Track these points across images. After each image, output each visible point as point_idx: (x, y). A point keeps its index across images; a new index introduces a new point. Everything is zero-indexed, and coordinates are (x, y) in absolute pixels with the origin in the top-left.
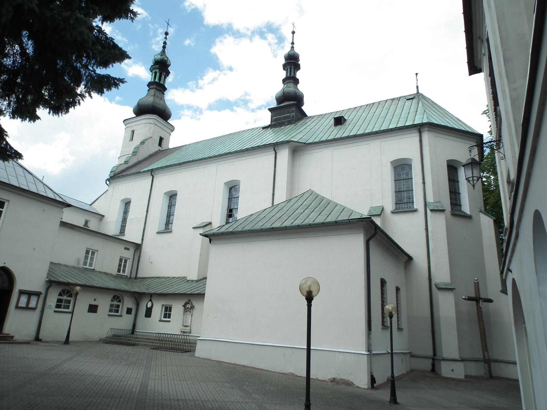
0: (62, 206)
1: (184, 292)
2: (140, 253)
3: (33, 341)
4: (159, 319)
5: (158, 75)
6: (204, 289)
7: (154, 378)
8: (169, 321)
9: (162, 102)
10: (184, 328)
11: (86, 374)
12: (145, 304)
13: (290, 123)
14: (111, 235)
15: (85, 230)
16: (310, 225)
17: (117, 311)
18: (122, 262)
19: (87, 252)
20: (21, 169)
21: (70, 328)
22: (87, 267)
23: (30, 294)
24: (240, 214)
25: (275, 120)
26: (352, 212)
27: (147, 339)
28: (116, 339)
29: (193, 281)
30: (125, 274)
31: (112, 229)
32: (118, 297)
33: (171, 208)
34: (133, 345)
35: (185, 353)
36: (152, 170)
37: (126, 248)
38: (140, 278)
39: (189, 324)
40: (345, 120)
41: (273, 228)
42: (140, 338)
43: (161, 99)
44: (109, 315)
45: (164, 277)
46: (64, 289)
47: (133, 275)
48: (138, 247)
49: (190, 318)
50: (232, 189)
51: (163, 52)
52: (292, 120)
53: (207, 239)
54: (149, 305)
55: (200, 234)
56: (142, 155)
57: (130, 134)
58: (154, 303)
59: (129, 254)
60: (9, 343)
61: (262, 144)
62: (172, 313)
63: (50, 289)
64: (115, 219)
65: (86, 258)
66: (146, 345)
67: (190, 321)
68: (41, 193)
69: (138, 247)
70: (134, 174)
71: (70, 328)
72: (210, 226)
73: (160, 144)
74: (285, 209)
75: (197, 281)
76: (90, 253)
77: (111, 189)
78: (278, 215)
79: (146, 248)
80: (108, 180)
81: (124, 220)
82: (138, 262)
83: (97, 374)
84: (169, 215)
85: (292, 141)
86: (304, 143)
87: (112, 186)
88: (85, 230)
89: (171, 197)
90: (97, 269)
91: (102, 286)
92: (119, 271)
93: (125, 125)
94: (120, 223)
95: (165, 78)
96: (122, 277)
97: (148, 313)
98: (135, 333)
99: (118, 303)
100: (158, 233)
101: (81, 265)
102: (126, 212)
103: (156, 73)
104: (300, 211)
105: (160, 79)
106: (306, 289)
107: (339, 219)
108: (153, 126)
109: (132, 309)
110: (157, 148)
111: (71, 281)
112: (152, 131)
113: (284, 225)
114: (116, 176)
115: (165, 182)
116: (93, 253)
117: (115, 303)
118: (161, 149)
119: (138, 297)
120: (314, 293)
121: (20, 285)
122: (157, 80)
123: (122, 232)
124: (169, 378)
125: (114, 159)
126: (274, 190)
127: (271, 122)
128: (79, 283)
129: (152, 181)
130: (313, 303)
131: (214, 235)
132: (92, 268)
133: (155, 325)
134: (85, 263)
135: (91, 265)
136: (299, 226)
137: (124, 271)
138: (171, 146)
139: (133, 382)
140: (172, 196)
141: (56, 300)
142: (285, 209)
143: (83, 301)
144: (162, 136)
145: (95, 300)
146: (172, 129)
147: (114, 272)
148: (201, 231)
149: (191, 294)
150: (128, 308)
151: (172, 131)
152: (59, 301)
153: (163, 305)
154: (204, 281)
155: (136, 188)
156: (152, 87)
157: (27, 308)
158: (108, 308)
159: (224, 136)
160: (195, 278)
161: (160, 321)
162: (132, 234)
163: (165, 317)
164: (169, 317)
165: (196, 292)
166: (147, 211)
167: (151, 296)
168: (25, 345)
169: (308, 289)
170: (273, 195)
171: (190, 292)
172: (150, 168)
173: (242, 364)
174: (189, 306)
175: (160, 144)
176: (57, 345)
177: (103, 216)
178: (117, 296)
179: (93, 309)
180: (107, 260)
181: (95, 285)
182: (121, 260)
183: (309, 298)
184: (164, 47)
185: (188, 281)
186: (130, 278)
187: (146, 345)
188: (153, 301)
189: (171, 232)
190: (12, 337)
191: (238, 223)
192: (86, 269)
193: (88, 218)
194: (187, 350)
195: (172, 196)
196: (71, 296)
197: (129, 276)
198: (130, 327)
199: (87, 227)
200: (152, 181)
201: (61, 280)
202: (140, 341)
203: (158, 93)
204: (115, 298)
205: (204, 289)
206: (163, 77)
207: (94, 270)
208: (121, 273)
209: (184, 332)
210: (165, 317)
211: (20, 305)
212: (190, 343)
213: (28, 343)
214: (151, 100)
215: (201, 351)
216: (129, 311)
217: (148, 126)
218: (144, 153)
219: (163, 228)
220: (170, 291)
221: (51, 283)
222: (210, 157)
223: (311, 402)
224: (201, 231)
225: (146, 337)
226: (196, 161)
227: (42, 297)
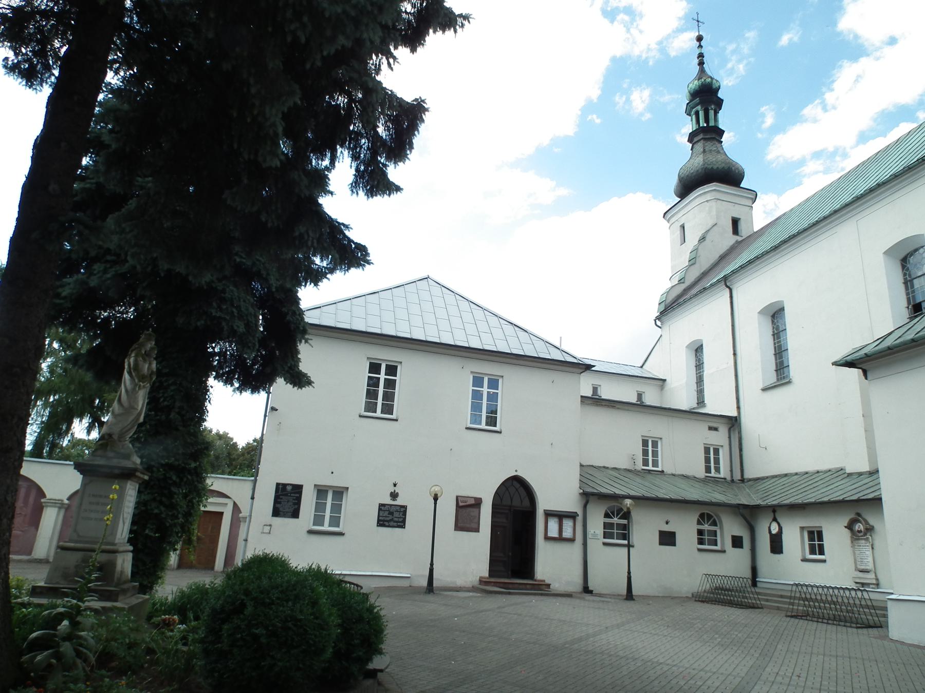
1: (841, 498)
2: (740, 432)
3: (581, 593)
4: (800, 558)
5: (701, 114)
6: (876, 482)
7: (771, 679)
8: (824, 561)
9: (720, 157)
10: (861, 575)
12: (765, 528)
15: (640, 406)
18: (710, 454)
19: (645, 443)
20: (511, 327)
21: (629, 573)
22: (650, 467)
23: (561, 516)
27: (782, 596)
28: (720, 595)
29: (860, 474)
30: (722, 475)
31: (683, 399)
32: (709, 517)
33: (779, 337)
34: (753, 607)
35: (865, 631)
36: (725, 278)
37: (710, 428)
38: (750, 480)
39: (870, 566)
42: (765, 595)
43: (718, 152)
45: (796, 474)
46: (613, 507)
47: (737, 476)
48: (733, 423)
49: (869, 553)
51: (702, 71)
53: (855, 373)
54: (775, 529)
56: (704, 263)
57: (678, 233)
58: (782, 525)
59: (720, 438)
60: (542, 595)
63: (588, 506)
64: (685, 380)
65: (645, 453)
66: (778, 608)
67: (870, 559)
68: (542, 356)
69: (733, 423)
70: (696, 295)
71: (629, 573)
73: (736, 231)
76: (649, 446)
77: (665, 332)
79: (747, 422)
80: (658, 318)
81: (700, 380)
82: (741, 450)
84: (780, 352)
87: (666, 327)
88: (640, 406)
89: (773, 316)
90: (668, 470)
91: (674, 497)
92: (708, 470)
93: (668, 221)
94: (694, 387)
95: (716, 113)
96: (716, 481)
97: (776, 545)
98: (759, 584)
99: (713, 528)
100: (765, 389)
101: (640, 466)
102: (699, 366)
103: (697, 113)
105: (707, 120)
108: (713, 203)
109: (741, 537)
110: (732, 239)
111: (618, 492)
112: (714, 213)
114: (670, 308)
115: (755, 292)
116: (655, 444)
117: (706, 527)
118: (740, 239)
119: (749, 514)
121: (544, 503)
122: (703, 124)
123: (701, 402)
124: (809, 683)
125: (661, 280)
128: (632, 493)
129: (731, 297)
132: (659, 469)
133: (791, 568)
134: (645, 463)
135: (655, 464)
137: (717, 470)
138: (757, 227)
139: (717, 684)
140: (776, 314)
143: (645, 528)
145: (667, 523)
147: (701, 473)
149: (858, 501)
152: (606, 525)
153: (802, 528)
155: (706, 319)
156: (696, 139)
157: (560, 539)
158: (695, 537)
159: (863, 163)
161: (804, 560)
162: (719, 402)
163: (813, 552)
164: (822, 552)
166: (735, 354)
167: (774, 511)
168: (564, 599)
174: (859, 527)
175: (736, 231)
176: (613, 601)
178: (708, 514)
179: (667, 539)
180: (683, 454)
182: (707, 450)
184: (701, 64)
185: (850, 475)
186: (733, 481)
187: (778, 608)
189: (789, 382)
190: (548, 585)
192: (649, 471)
193: (640, 389)
194: (871, 623)
195: (776, 314)
197: (729, 478)
198: (748, 574)
199: (642, 403)
200: (731, 297)
201: (603, 491)
202: (767, 600)
203: (709, 145)
205: (876, 482)
206: (712, 113)
207: (663, 471)
208: (713, 473)
209: (863, 584)
210: (813, 552)
211: (550, 534)
212: (874, 608)
213: (569, 595)
214: (699, 161)
216: (737, 542)
217: (707, 206)
218: (708, 258)
219: (772, 378)
220: (811, 498)
221: (588, 497)
222: (836, 212)
225: (780, 593)
226: (805, 230)
227: (579, 519)
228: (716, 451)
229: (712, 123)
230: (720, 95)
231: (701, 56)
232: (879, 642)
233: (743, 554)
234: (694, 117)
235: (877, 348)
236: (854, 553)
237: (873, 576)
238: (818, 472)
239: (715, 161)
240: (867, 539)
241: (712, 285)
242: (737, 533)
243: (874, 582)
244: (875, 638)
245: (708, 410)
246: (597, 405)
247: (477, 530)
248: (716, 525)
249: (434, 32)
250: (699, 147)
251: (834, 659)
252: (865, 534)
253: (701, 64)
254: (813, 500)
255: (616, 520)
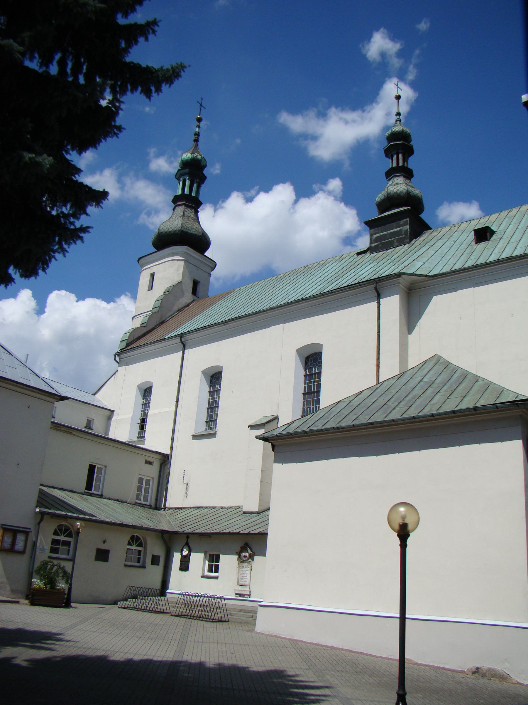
0: (52, 400)
1: (237, 531)
4: (201, 574)
5: (188, 183)
8: (217, 578)
9: (195, 225)
10: (241, 588)
11: (94, 647)
13: (401, 242)
14: (124, 440)
16: (432, 415)
17: (139, 561)
24: (327, 399)
25: (376, 240)
26: (502, 390)
29: (251, 513)
32: (138, 538)
36: (182, 335)
37: (147, 462)
38: (170, 509)
39: (247, 583)
40: (493, 233)
41: (372, 423)
44: (126, 565)
45: (206, 507)
49: (248, 572)
50: (312, 360)
52: (405, 238)
55: (257, 437)
61: (356, 282)
62: (221, 564)
63: (42, 524)
67: (248, 577)
69: (165, 460)
72: (276, 421)
74: (393, 391)
75: (258, 513)
77: (122, 369)
78: (382, 401)
80: (118, 354)
83: (108, 648)
84: (213, 407)
85: (405, 274)
86: (426, 276)
97: (184, 566)
100: (196, 437)
102: (146, 405)
104: (417, 391)
106: (397, 521)
107: (478, 404)
109: (160, 556)
113: (389, 418)
115: (202, 357)
120: (410, 527)
122: (186, 192)
123: (26, 362)
126: (378, 358)
127: (371, 243)
130: (409, 541)
131: (278, 437)
136: (414, 418)
141: (50, 541)
142: (393, 391)
144: (198, 279)
145: (104, 542)
146: (213, 265)
148: (260, 432)
150: (153, 556)
151: (213, 269)
152: (54, 542)
154: (265, 513)
155: (158, 369)
160: (256, 509)
161: (203, 577)
162: (156, 441)
163: (210, 570)
164: (217, 571)
165: (257, 531)
169: (401, 521)
170: (378, 366)
171: (246, 532)
172: (179, 331)
173: (329, 644)
177: (113, 411)
181: (104, 519)
182: (141, 480)
183: (403, 533)
185: (245, 513)
188: (190, 545)
191: (319, 414)
196: (70, 535)
200: (183, 357)
204: (134, 540)
206: (195, 186)
209: (241, 595)
210: (210, 570)
215: (264, 623)
216: (155, 560)
219: (202, 429)
223: (407, 689)
224: (260, 432)
228: (148, 482)
229: (193, 194)
230: (205, 172)
231: (197, 134)
232: (249, 633)
233: (157, 571)
234: (181, 183)
235: (284, 432)
236: (239, 572)
237: (248, 590)
238: (222, 508)
239: (191, 226)
240: (249, 562)
241: (170, 338)
242: (156, 553)
243: (248, 593)
244: (247, 631)
245: (147, 445)
246: (57, 430)
247: (158, 565)
248: (142, 546)
249: (102, 203)
250: (180, 210)
251: (224, 645)
252: (248, 559)
253: (196, 141)
254: (217, 531)
255: (62, 538)
